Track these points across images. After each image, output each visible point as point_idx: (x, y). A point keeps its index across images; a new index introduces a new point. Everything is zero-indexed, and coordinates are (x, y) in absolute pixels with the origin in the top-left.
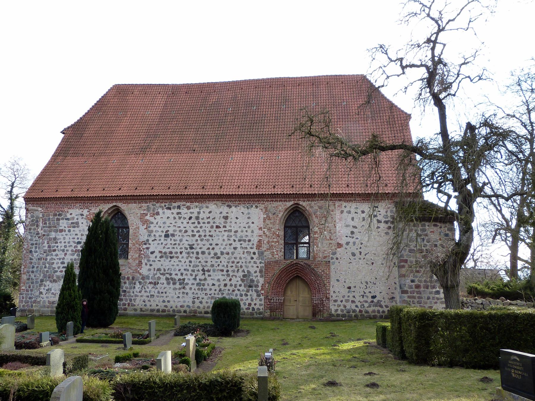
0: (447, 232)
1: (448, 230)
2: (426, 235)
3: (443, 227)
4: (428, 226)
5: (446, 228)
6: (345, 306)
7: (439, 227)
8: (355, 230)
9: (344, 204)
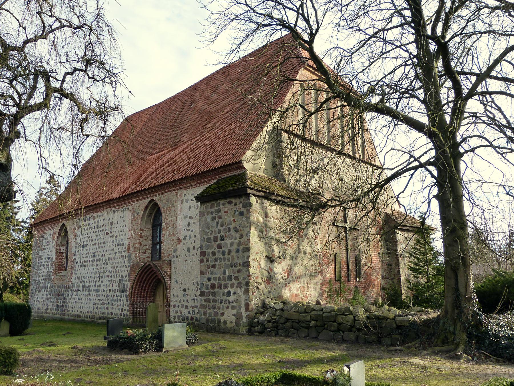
0: (242, 209)
1: (243, 207)
2: (220, 217)
3: (238, 203)
4: (223, 205)
5: (241, 205)
6: (181, 313)
7: (233, 204)
8: (191, 221)
9: (184, 192)
